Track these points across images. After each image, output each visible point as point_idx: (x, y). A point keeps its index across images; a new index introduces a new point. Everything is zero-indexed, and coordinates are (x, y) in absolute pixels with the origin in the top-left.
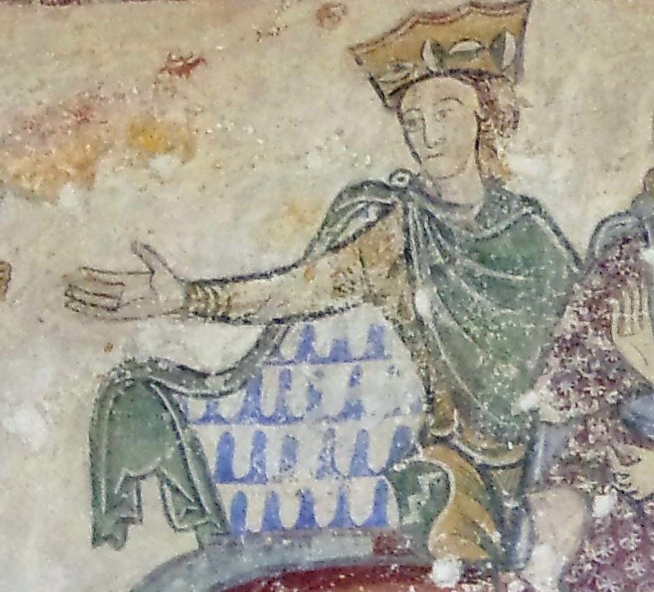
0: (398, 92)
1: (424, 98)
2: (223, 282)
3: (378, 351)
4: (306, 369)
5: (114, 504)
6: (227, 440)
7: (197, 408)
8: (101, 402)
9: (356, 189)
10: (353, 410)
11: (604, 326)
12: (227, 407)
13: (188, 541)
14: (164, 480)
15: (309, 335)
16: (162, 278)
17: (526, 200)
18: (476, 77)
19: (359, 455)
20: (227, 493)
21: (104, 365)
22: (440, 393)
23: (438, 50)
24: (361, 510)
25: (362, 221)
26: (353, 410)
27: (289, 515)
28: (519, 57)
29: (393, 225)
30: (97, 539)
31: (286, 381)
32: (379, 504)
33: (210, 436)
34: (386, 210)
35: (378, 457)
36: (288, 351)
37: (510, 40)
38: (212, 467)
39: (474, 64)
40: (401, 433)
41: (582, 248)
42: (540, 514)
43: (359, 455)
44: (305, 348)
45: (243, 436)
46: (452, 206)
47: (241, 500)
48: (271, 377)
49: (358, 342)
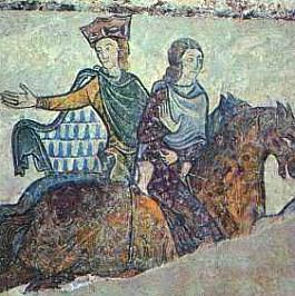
0: (95, 42)
1: (102, 44)
2: (48, 97)
3: (93, 119)
4: (73, 125)
5: (20, 162)
6: (52, 145)
7: (42, 135)
8: (14, 132)
9: (84, 71)
10: (87, 137)
11: (156, 114)
12: (51, 135)
13: (42, 175)
14: (34, 156)
15: (73, 115)
16: (30, 96)
17: (133, 76)
18: (117, 38)
19: (90, 149)
20: (52, 160)
21: (16, 119)
22: (111, 132)
23: (107, 31)
24: (91, 166)
25: (86, 81)
26: (87, 137)
27: (70, 168)
28: (129, 33)
29: (96, 80)
30: (16, 174)
31: (67, 127)
32: (96, 163)
33: (47, 143)
34: (93, 78)
35: (95, 151)
36: (68, 119)
37: (126, 27)
38: (210, 113)
39: (116, 34)
40: (101, 144)
41: (149, 90)
42: (141, 168)
43: (90, 149)
44: (72, 120)
45: (56, 143)
46: (112, 77)
47: (56, 162)
48: (63, 126)
49: (87, 115)
